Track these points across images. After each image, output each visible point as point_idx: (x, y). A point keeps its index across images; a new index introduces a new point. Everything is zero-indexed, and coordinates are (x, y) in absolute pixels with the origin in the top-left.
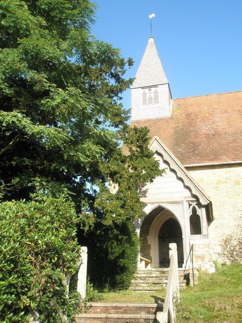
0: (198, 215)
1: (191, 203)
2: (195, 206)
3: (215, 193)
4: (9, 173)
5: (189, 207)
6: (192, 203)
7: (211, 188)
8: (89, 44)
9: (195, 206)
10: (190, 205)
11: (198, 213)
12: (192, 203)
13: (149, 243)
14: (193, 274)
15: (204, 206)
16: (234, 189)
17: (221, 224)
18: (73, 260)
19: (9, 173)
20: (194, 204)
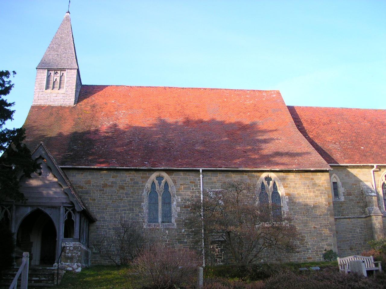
0: (73, 221)
1: (67, 208)
2: (71, 211)
3: (100, 195)
4: (14, 168)
5: (2, 212)
6: (68, 209)
7: (97, 191)
8: (196, 274)
9: (71, 211)
10: (66, 210)
11: (73, 218)
12: (68, 209)
13: (31, 241)
14: (341, 218)
15: (78, 212)
16: (118, 193)
17: (101, 226)
18: (101, 242)
19: (14, 168)
20: (70, 210)
